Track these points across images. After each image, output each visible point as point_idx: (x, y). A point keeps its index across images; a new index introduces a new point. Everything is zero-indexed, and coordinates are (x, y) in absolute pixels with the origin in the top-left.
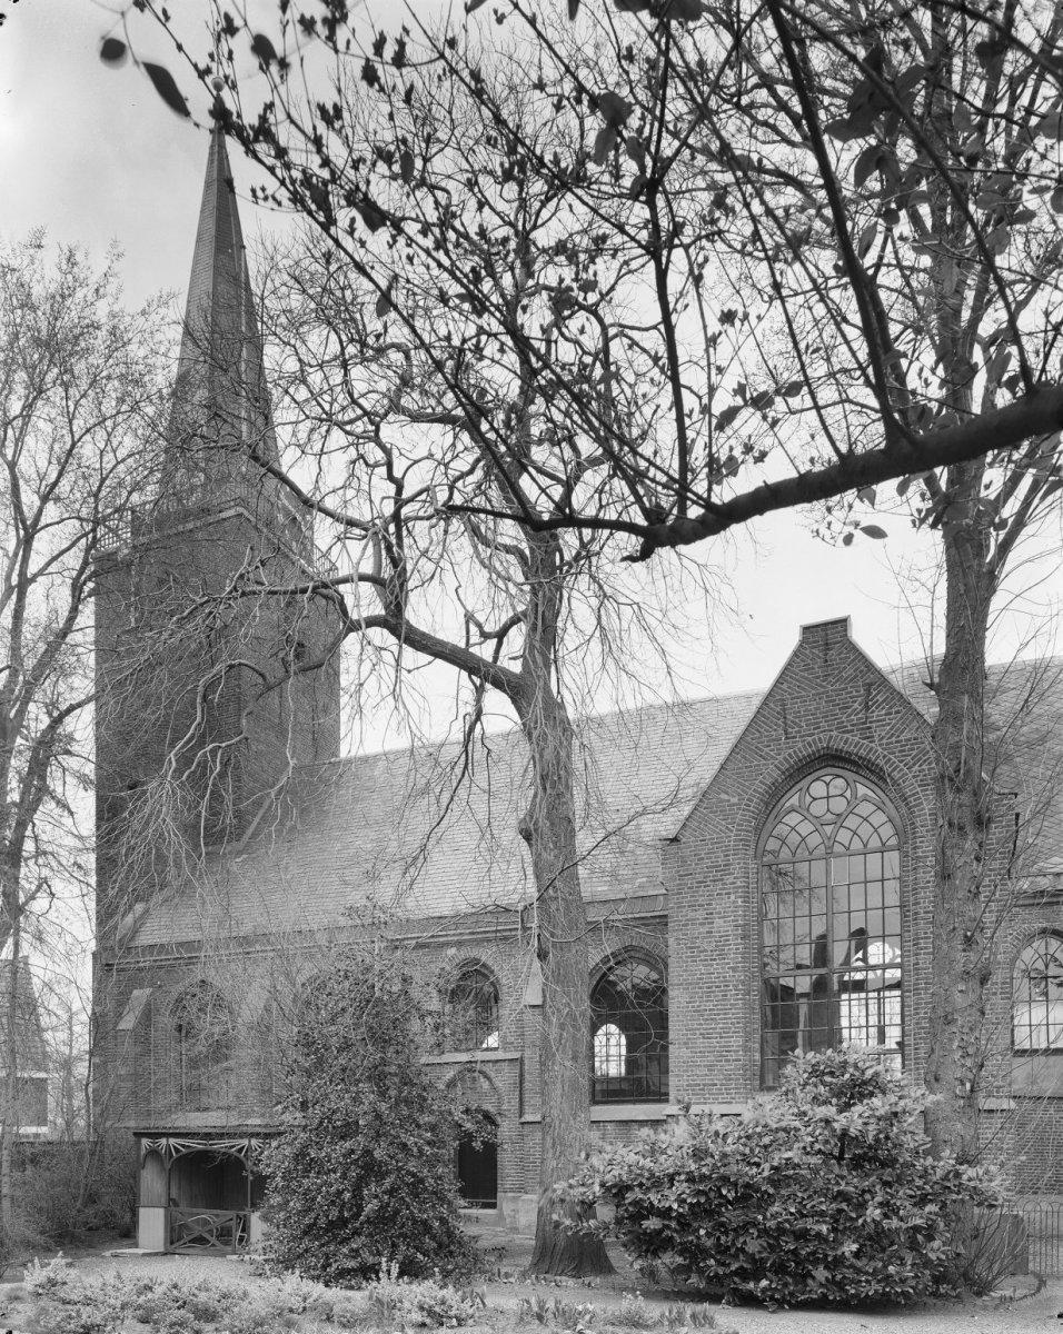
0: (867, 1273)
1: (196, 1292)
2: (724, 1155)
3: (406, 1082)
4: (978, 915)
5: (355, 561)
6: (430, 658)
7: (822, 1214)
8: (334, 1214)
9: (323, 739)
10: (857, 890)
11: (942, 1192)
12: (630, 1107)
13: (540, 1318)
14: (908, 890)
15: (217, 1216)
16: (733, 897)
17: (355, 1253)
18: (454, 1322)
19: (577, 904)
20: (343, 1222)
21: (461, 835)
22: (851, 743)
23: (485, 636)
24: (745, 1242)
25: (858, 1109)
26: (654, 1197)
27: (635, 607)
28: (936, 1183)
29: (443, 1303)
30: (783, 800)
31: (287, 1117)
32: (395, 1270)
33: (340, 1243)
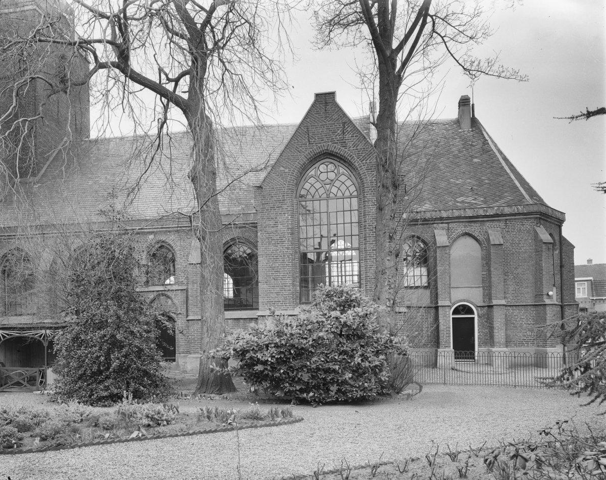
0: (356, 387)
1: (18, 414)
2: (292, 335)
3: (133, 300)
4: (395, 227)
5: (104, 28)
6: (143, 87)
7: (336, 361)
8: (95, 368)
9: (82, 128)
10: (340, 214)
11: (383, 349)
12: (239, 312)
13: (209, 417)
14: (362, 214)
15: (27, 371)
16: (286, 215)
17: (107, 388)
18: (165, 423)
19: (217, 214)
20: (100, 372)
21: (156, 181)
22: (336, 148)
23: (169, 80)
24: (302, 375)
25: (350, 312)
26: (259, 355)
27: (240, 76)
28: (382, 345)
29: (159, 413)
30: (308, 172)
31: (68, 319)
32: (131, 397)
33: (99, 383)
